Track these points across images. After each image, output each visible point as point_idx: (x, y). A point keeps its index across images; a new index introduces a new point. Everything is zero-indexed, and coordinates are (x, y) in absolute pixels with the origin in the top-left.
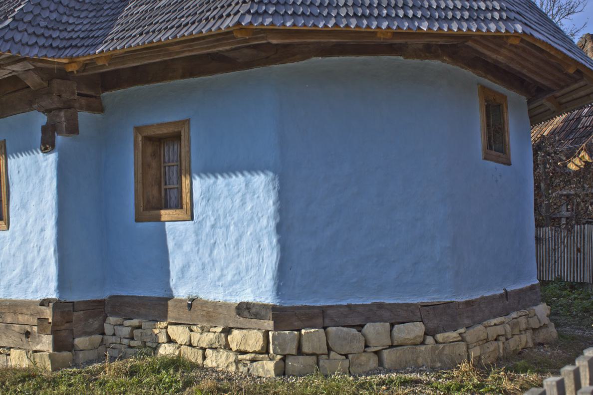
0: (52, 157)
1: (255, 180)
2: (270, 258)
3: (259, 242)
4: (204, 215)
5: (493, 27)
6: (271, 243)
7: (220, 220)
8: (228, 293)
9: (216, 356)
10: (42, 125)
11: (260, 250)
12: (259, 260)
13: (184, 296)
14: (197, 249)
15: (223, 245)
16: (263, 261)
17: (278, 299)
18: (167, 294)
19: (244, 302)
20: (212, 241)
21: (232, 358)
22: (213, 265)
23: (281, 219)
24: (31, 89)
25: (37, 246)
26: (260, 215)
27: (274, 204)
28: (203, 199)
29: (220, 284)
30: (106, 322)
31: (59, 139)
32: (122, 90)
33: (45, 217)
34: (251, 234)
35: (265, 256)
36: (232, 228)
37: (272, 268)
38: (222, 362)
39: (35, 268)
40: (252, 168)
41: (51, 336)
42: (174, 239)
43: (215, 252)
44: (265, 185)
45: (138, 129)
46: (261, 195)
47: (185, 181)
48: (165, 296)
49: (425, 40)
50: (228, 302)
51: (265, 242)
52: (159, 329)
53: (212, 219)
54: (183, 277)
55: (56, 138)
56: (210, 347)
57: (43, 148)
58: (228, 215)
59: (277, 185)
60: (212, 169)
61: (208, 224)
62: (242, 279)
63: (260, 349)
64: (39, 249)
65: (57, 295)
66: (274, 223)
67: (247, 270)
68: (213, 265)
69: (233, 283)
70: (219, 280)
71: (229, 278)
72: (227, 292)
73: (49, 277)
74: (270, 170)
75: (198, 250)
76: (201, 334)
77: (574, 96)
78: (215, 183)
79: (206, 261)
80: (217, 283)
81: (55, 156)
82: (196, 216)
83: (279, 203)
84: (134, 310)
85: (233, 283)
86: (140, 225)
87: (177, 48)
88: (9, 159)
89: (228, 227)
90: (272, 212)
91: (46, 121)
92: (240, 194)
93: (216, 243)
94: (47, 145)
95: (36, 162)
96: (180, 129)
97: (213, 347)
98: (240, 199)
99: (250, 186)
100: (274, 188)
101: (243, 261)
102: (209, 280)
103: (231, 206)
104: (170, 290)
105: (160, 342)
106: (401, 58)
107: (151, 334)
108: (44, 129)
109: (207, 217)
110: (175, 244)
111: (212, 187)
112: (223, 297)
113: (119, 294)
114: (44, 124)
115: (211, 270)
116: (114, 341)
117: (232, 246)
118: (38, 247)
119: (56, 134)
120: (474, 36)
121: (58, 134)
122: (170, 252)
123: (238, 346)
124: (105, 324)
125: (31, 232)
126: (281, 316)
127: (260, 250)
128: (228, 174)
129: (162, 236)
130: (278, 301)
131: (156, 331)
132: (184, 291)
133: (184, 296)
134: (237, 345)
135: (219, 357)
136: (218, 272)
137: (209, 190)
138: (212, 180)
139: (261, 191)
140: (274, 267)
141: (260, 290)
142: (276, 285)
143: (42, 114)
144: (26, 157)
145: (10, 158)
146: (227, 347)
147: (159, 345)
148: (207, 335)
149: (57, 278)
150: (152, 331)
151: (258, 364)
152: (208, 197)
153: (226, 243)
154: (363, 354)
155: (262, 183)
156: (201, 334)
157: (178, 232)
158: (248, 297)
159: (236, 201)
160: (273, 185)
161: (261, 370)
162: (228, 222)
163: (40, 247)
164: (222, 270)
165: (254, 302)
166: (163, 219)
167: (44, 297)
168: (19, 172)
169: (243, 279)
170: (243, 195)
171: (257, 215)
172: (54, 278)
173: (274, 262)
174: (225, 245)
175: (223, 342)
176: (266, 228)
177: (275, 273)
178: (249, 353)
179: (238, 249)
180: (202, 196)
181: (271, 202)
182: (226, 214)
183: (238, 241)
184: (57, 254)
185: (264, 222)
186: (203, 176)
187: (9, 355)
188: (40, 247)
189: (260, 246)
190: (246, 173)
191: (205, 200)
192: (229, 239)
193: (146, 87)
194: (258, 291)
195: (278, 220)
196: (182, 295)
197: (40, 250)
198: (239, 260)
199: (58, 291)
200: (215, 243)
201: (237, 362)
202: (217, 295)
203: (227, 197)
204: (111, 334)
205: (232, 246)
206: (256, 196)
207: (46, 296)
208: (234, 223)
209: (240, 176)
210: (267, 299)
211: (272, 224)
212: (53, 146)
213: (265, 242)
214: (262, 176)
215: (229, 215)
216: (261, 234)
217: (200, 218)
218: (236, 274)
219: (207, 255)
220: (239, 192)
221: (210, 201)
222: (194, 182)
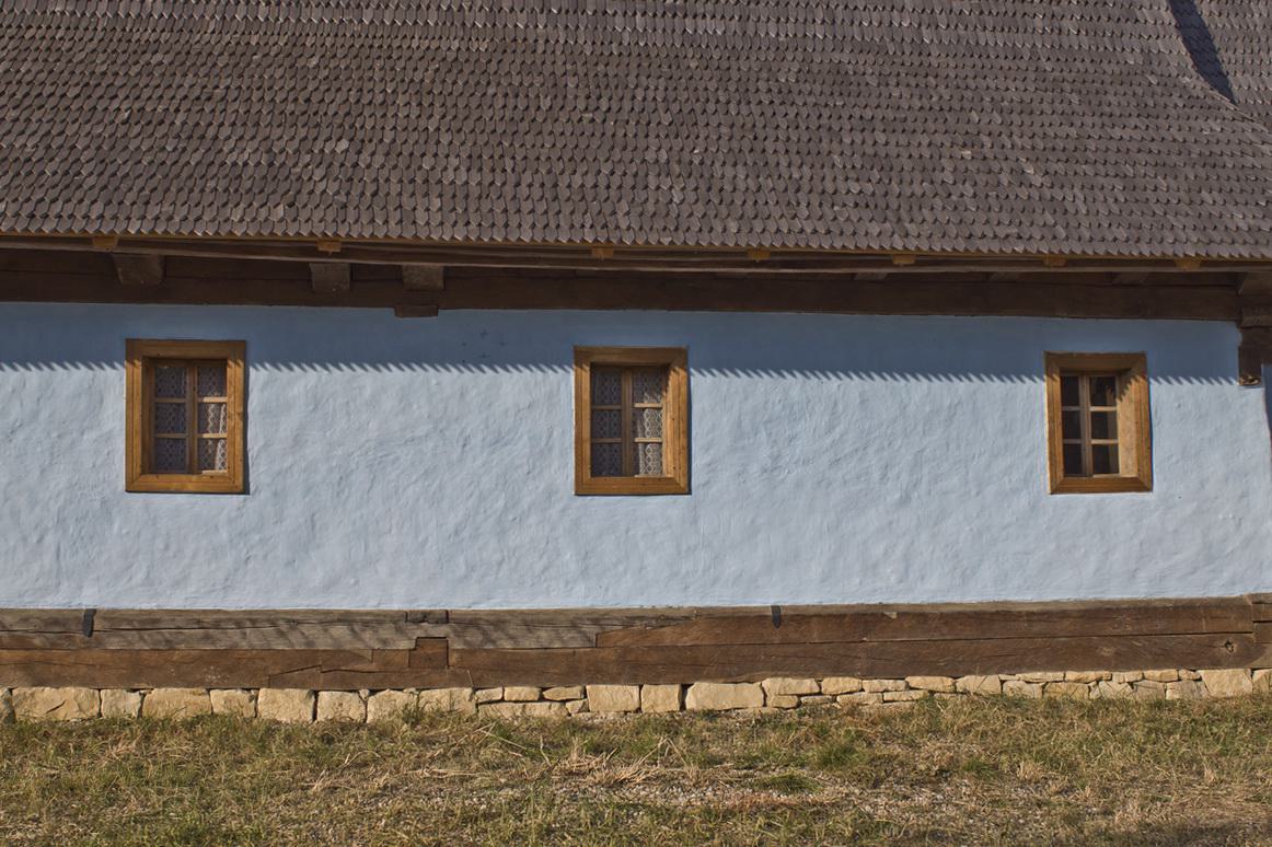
25: (1234, 518)
39: (1230, 548)
88: (251, 369)
94: (1249, 376)
163: (1240, 519)
188: (1240, 519)
197: (1240, 524)
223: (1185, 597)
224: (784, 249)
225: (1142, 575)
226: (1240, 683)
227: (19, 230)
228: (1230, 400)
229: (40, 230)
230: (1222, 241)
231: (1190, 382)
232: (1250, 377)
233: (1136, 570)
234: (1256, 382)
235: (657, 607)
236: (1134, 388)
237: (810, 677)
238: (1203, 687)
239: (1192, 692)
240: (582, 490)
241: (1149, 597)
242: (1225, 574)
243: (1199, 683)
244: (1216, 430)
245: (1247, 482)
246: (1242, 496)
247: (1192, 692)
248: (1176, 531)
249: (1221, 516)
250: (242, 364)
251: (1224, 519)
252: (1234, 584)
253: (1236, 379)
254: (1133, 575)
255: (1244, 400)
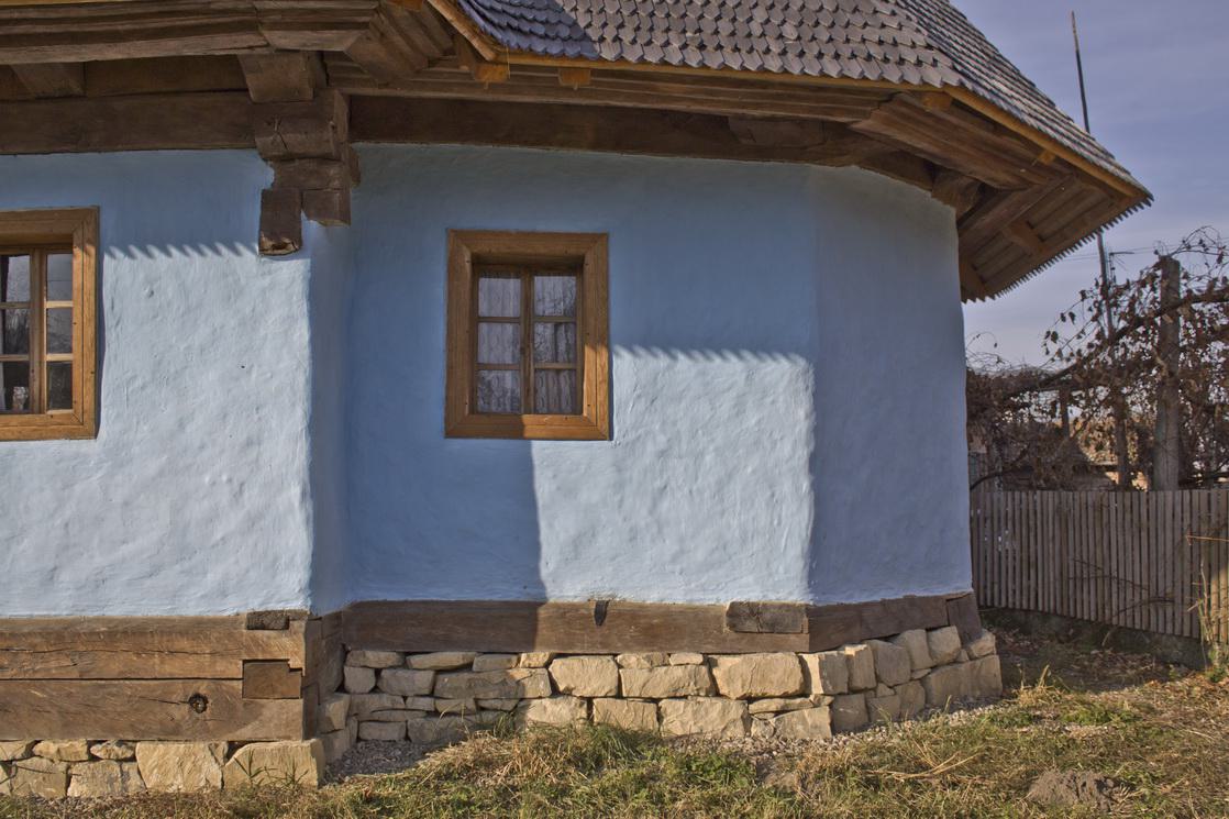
1: (769, 369)
2: (796, 519)
3: (771, 487)
4: (641, 431)
6: (798, 489)
7: (680, 441)
8: (697, 586)
9: (695, 713)
11: (773, 501)
12: (772, 523)
13: (576, 597)
14: (618, 497)
15: (686, 490)
16: (779, 524)
17: (811, 592)
18: (528, 594)
19: (741, 603)
20: (658, 484)
21: (736, 710)
22: (660, 531)
23: (816, 447)
24: (249, 96)
25: (230, 480)
26: (776, 436)
27: (807, 417)
28: (639, 397)
29: (678, 568)
30: (348, 663)
32: (414, 145)
34: (754, 472)
35: (783, 514)
36: (708, 458)
37: (800, 536)
38: (713, 722)
39: (218, 536)
40: (763, 345)
41: (301, 701)
42: (555, 476)
43: (665, 505)
44: (790, 381)
45: (459, 236)
46: (781, 399)
47: (593, 360)
48: (522, 599)
50: (697, 604)
51: (786, 487)
52: (526, 667)
53: (662, 439)
55: (303, 226)
56: (672, 694)
57: (268, 244)
58: (700, 432)
59: (811, 382)
60: (667, 336)
61: (650, 448)
62: (730, 558)
63: (798, 688)
64: (237, 489)
66: (805, 453)
67: (744, 541)
68: (660, 531)
69: (708, 566)
70: (674, 559)
71: (700, 555)
72: (693, 585)
73: (276, 559)
74: (802, 355)
75: (621, 501)
76: (651, 670)
78: (669, 368)
79: (643, 523)
80: (669, 568)
81: (302, 268)
82: (619, 431)
84: (434, 631)
85: (708, 566)
86: (457, 444)
87: (676, 89)
88: (107, 258)
89: (699, 456)
90: (804, 430)
91: (272, 181)
92: (733, 393)
93: (668, 488)
94: (279, 239)
95: (225, 276)
96: (583, 251)
97: (678, 695)
98: (733, 403)
99: (756, 379)
100: (807, 388)
101: (734, 523)
102: (648, 562)
103: (708, 416)
104: (540, 585)
105: (528, 696)
107: (504, 682)
108: (269, 199)
109: (646, 435)
110: (559, 488)
111: (663, 375)
112: (686, 595)
115: (653, 541)
116: (388, 704)
117: (707, 495)
118: (236, 484)
119: (303, 214)
121: (309, 217)
122: (540, 503)
123: (747, 688)
124: (346, 669)
126: (824, 626)
127: (773, 501)
128: (703, 353)
130: (811, 596)
131: (519, 673)
133: (576, 597)
134: (743, 687)
135: (703, 713)
136: (670, 546)
137: (656, 379)
138: (663, 361)
139: (781, 390)
141: (781, 580)
142: (807, 568)
145: (112, 256)
146: (714, 692)
147: (522, 704)
148: (666, 672)
150: (507, 674)
151: (793, 716)
152: (651, 396)
153: (695, 488)
154: (910, 684)
155: (782, 376)
156: (651, 670)
157: (568, 462)
158: (749, 590)
159: (720, 406)
160: (805, 382)
161: (800, 727)
162: (701, 447)
163: (242, 485)
164: (681, 540)
165: (763, 600)
166: (527, 435)
167: (256, 605)
169: (734, 558)
170: (738, 397)
171: (771, 434)
172: (298, 559)
173: (804, 525)
174: (691, 492)
175: (705, 682)
176: (787, 461)
177: (806, 545)
178: (772, 697)
179: (722, 500)
180: (638, 392)
181: (801, 413)
182: (697, 431)
183: (720, 486)
184: (309, 505)
185: (786, 448)
186: (642, 352)
187: (133, 759)
188: (242, 485)
189: (773, 495)
190: (747, 354)
191: (643, 400)
192: (700, 480)
193: (489, 150)
194: (771, 580)
195: (812, 447)
197: (241, 492)
198: (724, 520)
199: (309, 592)
200: (665, 487)
201: (747, 720)
202: (668, 592)
203: (699, 398)
204: (367, 690)
205: (707, 495)
206: (768, 400)
207: (261, 605)
208: (716, 450)
209: (733, 359)
210: (791, 593)
211: (803, 454)
212: (298, 241)
213: (786, 487)
214: (784, 363)
215: (704, 434)
216: (777, 471)
217: (632, 436)
218: (717, 548)
219: (644, 512)
220: (729, 389)
221: (658, 403)
222: (616, 362)
223: (139, 615)
225: (65, 577)
226: (197, 768)
228: (243, 281)
233: (55, 569)
236: (81, 260)
237: (332, 744)
238: (133, 773)
239: (111, 781)
240: (602, 431)
241: (78, 615)
242: (210, 576)
243: (126, 766)
246: (249, 443)
247: (111, 781)
248: (126, 504)
249: (207, 479)
250: (92, 250)
252: (224, 594)
254: (51, 576)
255: (268, 280)
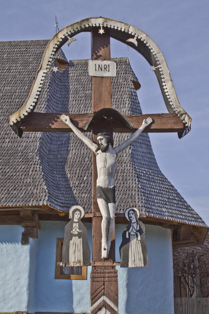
0: (27, 248)
5: (152, 215)
10: (22, 232)
17: (126, 312)
23: (128, 282)
25: (14, 286)
27: (126, 276)
31: (31, 240)
33: (20, 274)
39: (11, 297)
42: (76, 287)
49: (171, 223)
54: (79, 304)
65: (26, 310)
73: (21, 301)
77: (27, 224)
83: (128, 276)
90: (125, 279)
94: (25, 241)
100: (126, 270)
104: (73, 309)
106: (161, 227)
108: (23, 234)
110: (76, 290)
113: (41, 311)
114: (23, 232)
118: (15, 287)
119: (29, 237)
120: (152, 218)
121: (30, 237)
125: (9, 280)
129: (71, 286)
132: (80, 310)
140: (125, 300)
143: (22, 227)
144: (15, 245)
149: (27, 302)
163: (16, 287)
168: (1, 251)
173: (125, 298)
184: (28, 291)
188: (16, 287)
195: (127, 282)
196: (78, 311)
197: (16, 288)
210: (122, 313)
224: (28, 206)
227: (14, 206)
229: (9, 205)
230: (62, 199)
231: (6, 244)
232: (24, 242)
234: (26, 244)
235: (114, 305)
242: (9, 304)
244: (12, 258)
245: (20, 275)
249: (10, 286)
251: (11, 287)
253: (20, 243)
